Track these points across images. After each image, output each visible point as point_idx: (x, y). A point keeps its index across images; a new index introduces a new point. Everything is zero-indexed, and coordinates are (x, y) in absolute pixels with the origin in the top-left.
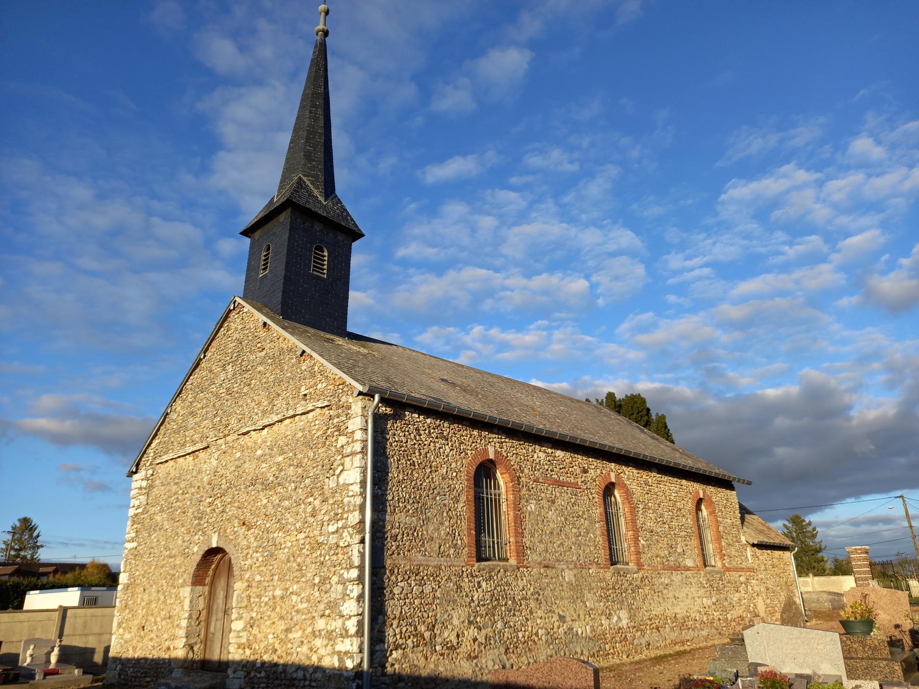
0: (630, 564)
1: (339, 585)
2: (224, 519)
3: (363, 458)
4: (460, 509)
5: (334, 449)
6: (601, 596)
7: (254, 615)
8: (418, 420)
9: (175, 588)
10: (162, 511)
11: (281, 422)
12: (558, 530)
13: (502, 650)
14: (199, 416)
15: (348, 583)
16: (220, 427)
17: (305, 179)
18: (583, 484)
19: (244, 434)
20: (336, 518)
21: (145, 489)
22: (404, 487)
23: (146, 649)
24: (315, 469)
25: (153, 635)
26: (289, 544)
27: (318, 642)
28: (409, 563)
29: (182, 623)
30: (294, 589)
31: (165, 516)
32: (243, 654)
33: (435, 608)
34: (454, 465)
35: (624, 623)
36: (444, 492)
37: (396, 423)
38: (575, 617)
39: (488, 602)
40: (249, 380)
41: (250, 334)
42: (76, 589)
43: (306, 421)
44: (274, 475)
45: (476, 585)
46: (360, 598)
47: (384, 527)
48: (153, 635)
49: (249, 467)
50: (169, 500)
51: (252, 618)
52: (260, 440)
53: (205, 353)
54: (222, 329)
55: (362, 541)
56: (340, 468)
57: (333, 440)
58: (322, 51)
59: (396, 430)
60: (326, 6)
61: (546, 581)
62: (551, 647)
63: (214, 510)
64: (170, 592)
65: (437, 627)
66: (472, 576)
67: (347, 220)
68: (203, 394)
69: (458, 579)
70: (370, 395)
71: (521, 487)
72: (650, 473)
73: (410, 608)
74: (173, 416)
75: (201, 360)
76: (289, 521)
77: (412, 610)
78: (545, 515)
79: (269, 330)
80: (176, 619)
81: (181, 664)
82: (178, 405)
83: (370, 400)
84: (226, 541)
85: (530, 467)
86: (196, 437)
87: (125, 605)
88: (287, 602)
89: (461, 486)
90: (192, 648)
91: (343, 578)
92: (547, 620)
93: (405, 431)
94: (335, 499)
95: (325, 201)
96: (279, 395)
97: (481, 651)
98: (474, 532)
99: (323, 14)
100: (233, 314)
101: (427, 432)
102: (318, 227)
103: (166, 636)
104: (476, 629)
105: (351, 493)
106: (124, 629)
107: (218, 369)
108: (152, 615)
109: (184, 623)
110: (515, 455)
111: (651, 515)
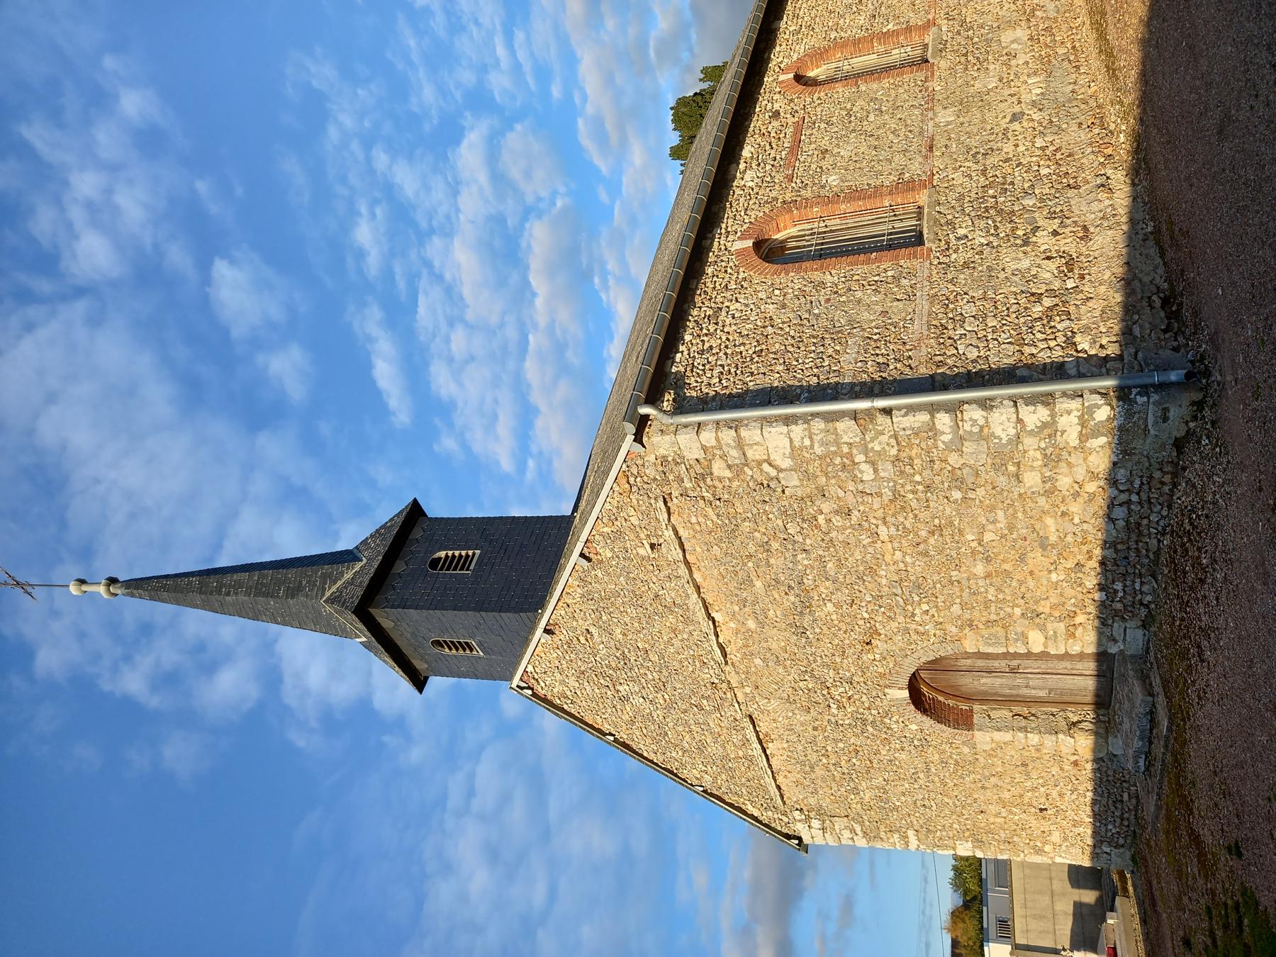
0: (926, 42)
1: (964, 449)
2: (862, 679)
3: (747, 425)
4: (836, 278)
5: (736, 484)
6: (978, 69)
7: (1018, 611)
8: (686, 353)
9: (977, 759)
10: (856, 791)
11: (699, 588)
12: (871, 139)
13: (1071, 193)
14: (703, 737)
15: (961, 432)
16: (718, 698)
17: (328, 594)
18: (796, 115)
19: (725, 655)
20: (849, 467)
21: (824, 822)
22: (798, 361)
23: (1077, 803)
24: (770, 516)
25: (1055, 794)
26: (898, 554)
27: (1064, 482)
28: (925, 341)
29: (1034, 743)
30: (974, 538)
31: (864, 784)
32: (1084, 628)
33: (1003, 296)
34: (762, 295)
35: (1021, 33)
36: (805, 304)
37: (690, 384)
38: (1015, 99)
39: (990, 222)
40: (639, 653)
41: (567, 658)
42: (986, 949)
43: (693, 541)
44: (786, 594)
45: (963, 242)
46: (985, 404)
47: (864, 383)
48: (1055, 794)
49: (778, 640)
50: (838, 779)
51: (1023, 614)
52: (732, 625)
53: (605, 734)
54: (565, 707)
55: (888, 412)
56: (766, 467)
57: (720, 486)
58: (137, 586)
59: (702, 382)
60: (72, 583)
61: (954, 146)
62: (1064, 126)
63: (849, 698)
64: (984, 768)
65: (1034, 290)
66: (947, 249)
67: (392, 526)
68: (669, 732)
69: (952, 269)
70: (643, 422)
71: (799, 199)
72: (781, 30)
73: (1003, 331)
74: (707, 781)
75: (616, 740)
76: (859, 557)
77: (1005, 328)
78: (847, 160)
79: (557, 624)
80: (1028, 754)
81: (1100, 740)
82: (689, 774)
83: (650, 425)
84: (897, 673)
85: (768, 189)
86: (737, 738)
87: (1006, 844)
88: (995, 550)
89: (796, 281)
90: (1074, 724)
91: (951, 441)
92: (1020, 138)
93: (703, 370)
94: (819, 473)
95: (362, 561)
96: (657, 596)
97: (1075, 222)
98: (874, 254)
99: (84, 588)
100: (540, 690)
101: (705, 338)
102: (399, 567)
103: (1055, 770)
104: (1037, 234)
105: (807, 442)
106: (1045, 843)
107: (629, 709)
108: (1021, 796)
109: (1034, 739)
110: (748, 212)
111: (847, 21)
